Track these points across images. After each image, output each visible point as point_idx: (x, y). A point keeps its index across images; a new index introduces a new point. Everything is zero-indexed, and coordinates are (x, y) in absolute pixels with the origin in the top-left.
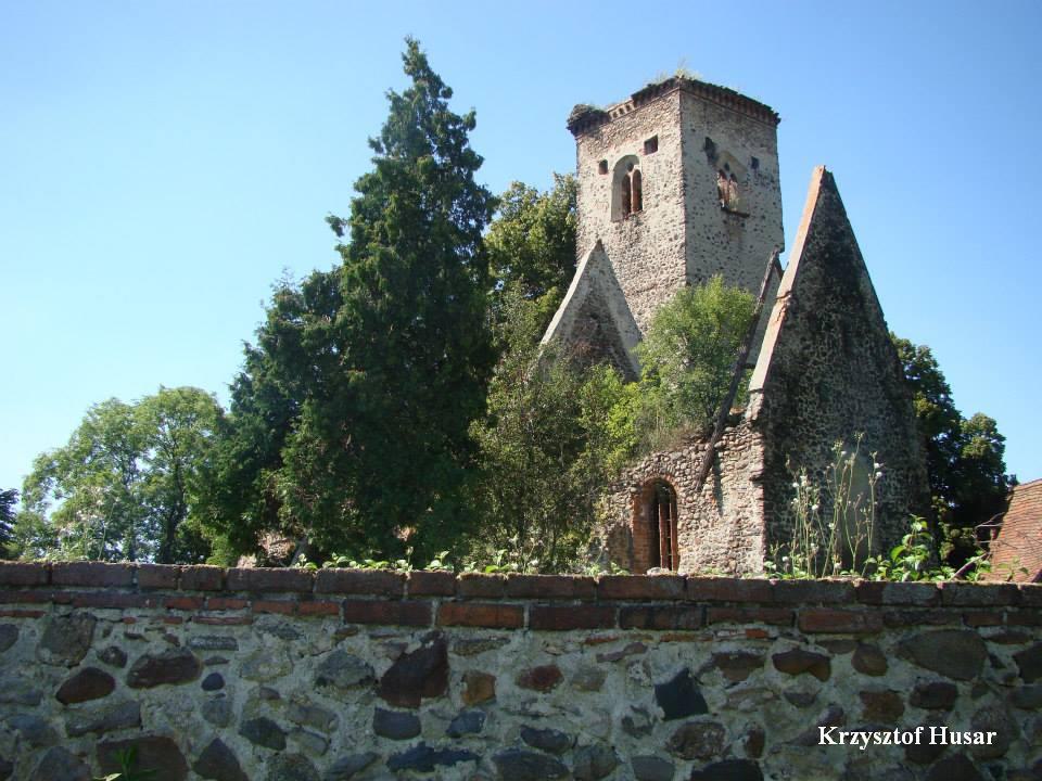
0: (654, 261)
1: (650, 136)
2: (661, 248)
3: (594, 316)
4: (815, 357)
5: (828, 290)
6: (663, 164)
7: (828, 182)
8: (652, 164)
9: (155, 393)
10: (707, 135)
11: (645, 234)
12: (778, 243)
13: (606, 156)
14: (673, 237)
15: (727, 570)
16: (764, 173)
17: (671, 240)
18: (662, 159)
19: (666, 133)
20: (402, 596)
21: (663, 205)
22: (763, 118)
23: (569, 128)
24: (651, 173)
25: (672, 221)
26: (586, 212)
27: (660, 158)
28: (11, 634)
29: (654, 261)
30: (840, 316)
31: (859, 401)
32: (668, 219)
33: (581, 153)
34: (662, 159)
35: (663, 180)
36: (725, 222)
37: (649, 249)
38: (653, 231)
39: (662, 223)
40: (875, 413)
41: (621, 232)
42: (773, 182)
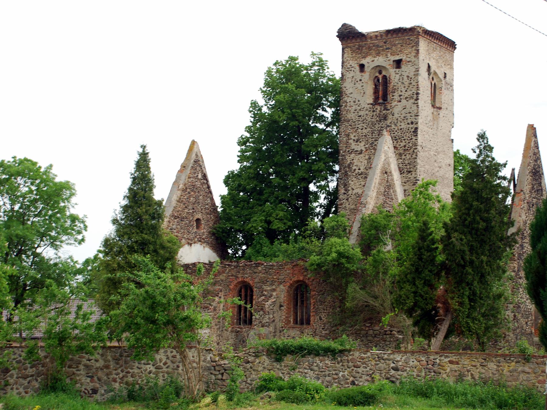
0: (396, 133)
1: (397, 58)
2: (401, 127)
3: (386, 173)
6: (405, 78)
9: (43, 164)
10: (428, 62)
13: (363, 62)
14: (409, 122)
15: (179, 297)
16: (448, 82)
17: (408, 124)
18: (405, 74)
19: (408, 59)
21: (404, 102)
22: (452, 45)
24: (396, 80)
25: (410, 113)
27: (404, 74)
28: (1, 313)
29: (396, 133)
32: (407, 110)
33: (346, 55)
34: (405, 74)
35: (404, 87)
36: (433, 113)
37: (393, 126)
38: (396, 116)
39: (403, 112)
41: (373, 111)
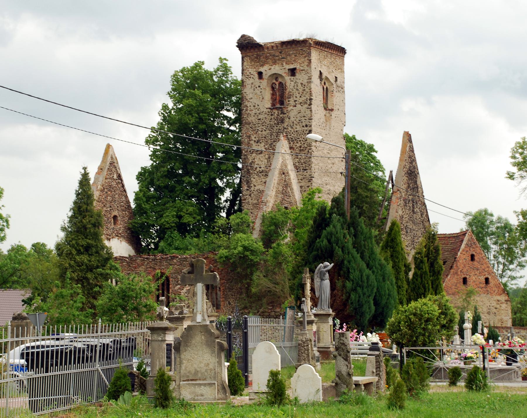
1: (292, 67)
3: (284, 173)
4: (405, 216)
5: (409, 187)
7: (408, 138)
8: (293, 83)
10: (320, 69)
11: (287, 120)
12: (343, 122)
13: (262, 69)
17: (303, 126)
18: (299, 82)
19: (302, 68)
20: (71, 293)
23: (237, 46)
24: (291, 87)
25: (304, 117)
26: (248, 98)
27: (298, 81)
29: (293, 135)
30: (412, 197)
31: (416, 231)
32: (302, 114)
34: (299, 82)
38: (292, 119)
39: (298, 116)
40: (420, 235)
42: (342, 88)
